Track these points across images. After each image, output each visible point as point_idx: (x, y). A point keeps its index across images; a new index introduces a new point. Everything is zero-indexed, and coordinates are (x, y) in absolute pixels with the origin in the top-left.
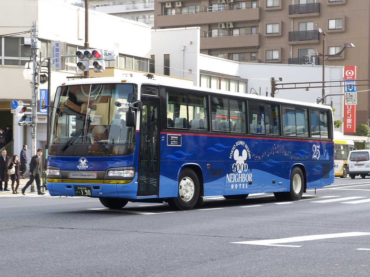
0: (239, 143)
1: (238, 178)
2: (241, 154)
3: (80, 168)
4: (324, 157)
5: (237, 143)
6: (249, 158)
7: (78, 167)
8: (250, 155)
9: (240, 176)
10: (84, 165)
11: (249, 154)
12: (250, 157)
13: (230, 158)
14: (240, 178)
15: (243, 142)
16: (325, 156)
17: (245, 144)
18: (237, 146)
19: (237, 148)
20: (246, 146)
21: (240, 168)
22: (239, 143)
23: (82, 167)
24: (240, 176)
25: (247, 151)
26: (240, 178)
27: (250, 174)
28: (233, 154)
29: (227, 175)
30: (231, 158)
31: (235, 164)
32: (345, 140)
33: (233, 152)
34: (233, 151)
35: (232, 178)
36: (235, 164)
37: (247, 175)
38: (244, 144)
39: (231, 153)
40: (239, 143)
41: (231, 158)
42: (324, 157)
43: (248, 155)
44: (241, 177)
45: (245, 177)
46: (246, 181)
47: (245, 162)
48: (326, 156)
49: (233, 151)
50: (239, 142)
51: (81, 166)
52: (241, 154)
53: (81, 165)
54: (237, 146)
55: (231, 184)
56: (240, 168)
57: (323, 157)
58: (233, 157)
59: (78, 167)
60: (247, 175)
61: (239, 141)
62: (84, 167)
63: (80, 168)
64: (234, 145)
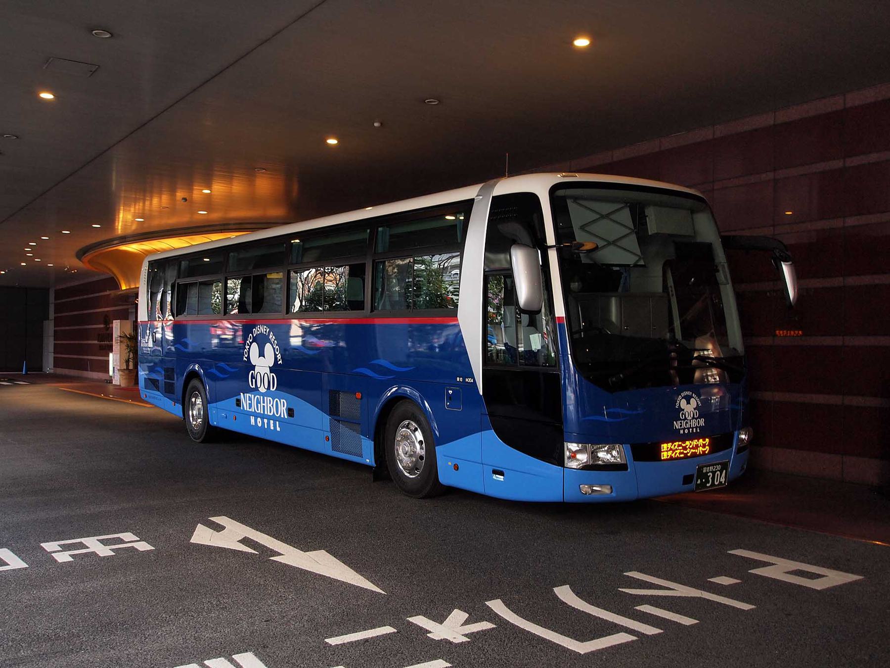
0: (259, 329)
1: (259, 405)
2: (262, 354)
3: (684, 429)
4: (146, 343)
5: (254, 329)
6: (279, 363)
7: (677, 425)
8: (279, 356)
9: (264, 403)
10: (693, 418)
11: (277, 353)
12: (280, 360)
13: (245, 359)
14: (264, 406)
15: (265, 327)
16: (147, 341)
17: (269, 332)
18: (255, 335)
19: (255, 340)
20: (271, 337)
21: (262, 380)
22: (258, 331)
23: (688, 426)
24: (264, 403)
25: (273, 347)
26: (264, 406)
27: (282, 400)
28: (249, 352)
29: (242, 394)
30: (246, 360)
31: (253, 372)
32: (720, 269)
33: (249, 349)
34: (248, 347)
35: (250, 402)
36: (252, 373)
37: (277, 401)
38: (268, 331)
39: (246, 350)
40: (259, 329)
41: (246, 360)
42: (146, 343)
43: (276, 355)
44: (265, 405)
45: (273, 405)
46: (276, 415)
47: (272, 370)
48: (148, 340)
49: (248, 347)
50: (259, 328)
51: (684, 423)
52: (262, 354)
53: (686, 419)
54: (255, 335)
55: (250, 414)
56: (262, 380)
57: (144, 342)
58: (248, 358)
59: (677, 425)
60: (277, 401)
61: (259, 326)
62: (694, 423)
63: (684, 429)
64: (251, 335)
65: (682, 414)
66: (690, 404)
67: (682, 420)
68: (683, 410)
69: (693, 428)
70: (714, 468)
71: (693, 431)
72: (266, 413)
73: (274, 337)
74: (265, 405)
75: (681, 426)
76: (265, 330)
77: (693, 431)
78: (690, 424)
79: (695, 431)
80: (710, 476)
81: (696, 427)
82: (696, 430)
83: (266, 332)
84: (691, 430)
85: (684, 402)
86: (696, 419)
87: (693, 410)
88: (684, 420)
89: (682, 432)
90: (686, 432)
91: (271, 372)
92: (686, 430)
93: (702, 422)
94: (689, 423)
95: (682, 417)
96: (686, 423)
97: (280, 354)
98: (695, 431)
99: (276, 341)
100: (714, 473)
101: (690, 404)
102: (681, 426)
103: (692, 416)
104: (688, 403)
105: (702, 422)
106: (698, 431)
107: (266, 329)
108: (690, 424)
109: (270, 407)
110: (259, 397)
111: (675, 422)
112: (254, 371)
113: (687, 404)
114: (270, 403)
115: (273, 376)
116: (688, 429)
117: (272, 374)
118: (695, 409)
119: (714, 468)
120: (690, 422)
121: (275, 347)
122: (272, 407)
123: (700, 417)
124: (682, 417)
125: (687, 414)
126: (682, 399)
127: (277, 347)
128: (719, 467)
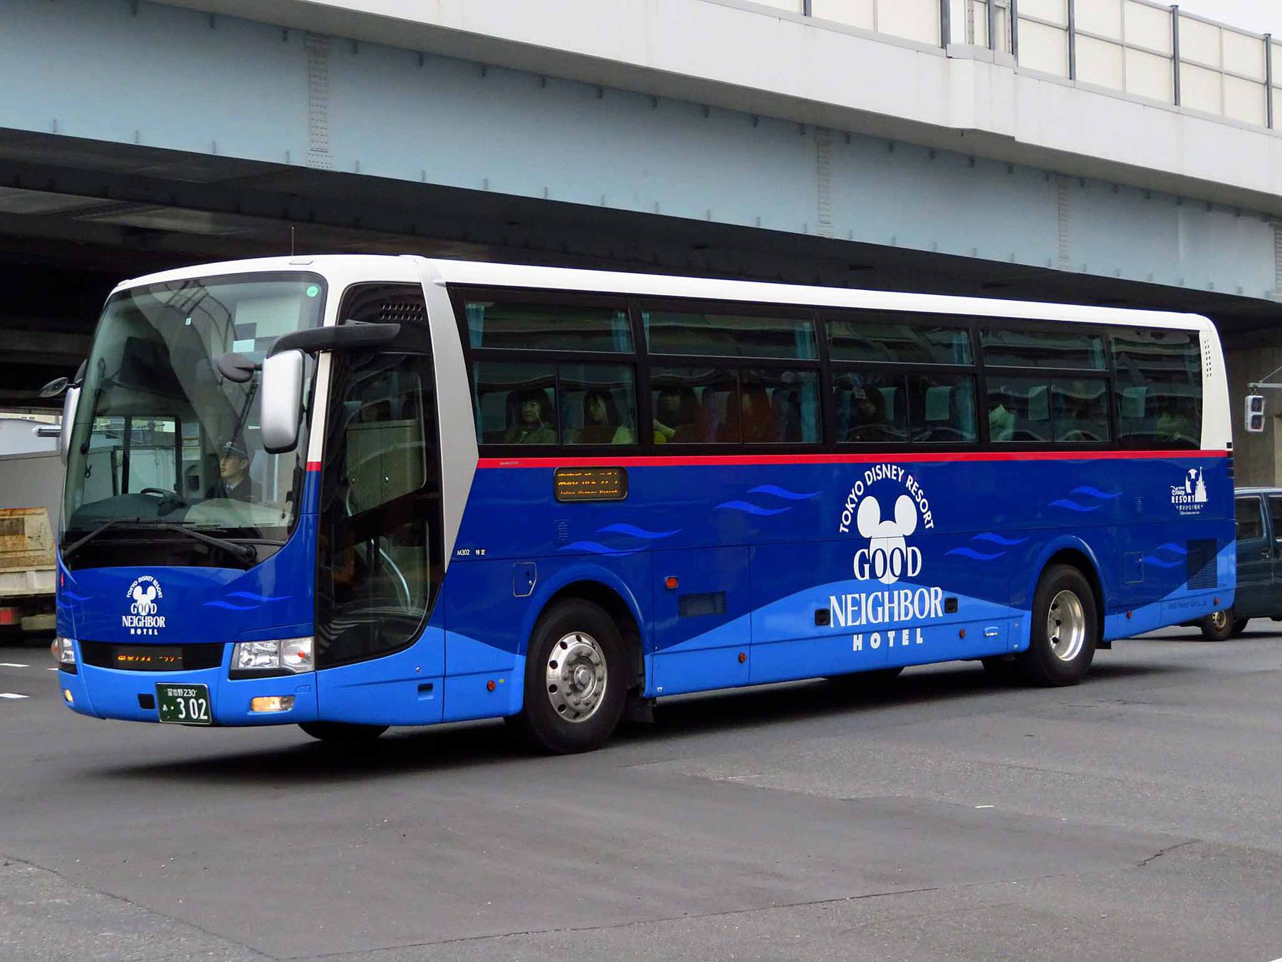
7: (126, 621)
10: (149, 614)
11: (923, 511)
12: (929, 522)
15: (894, 467)
16: (1189, 490)
20: (909, 484)
23: (141, 624)
27: (933, 590)
44: (895, 605)
45: (912, 603)
50: (881, 469)
53: (138, 614)
56: (889, 562)
62: (150, 622)
63: (136, 628)
65: (135, 607)
66: (146, 593)
67: (133, 615)
68: (136, 601)
69: (148, 628)
70: (184, 692)
71: (147, 632)
72: (896, 619)
73: (916, 484)
74: (146, 621)
75: (132, 623)
76: (894, 472)
77: (147, 632)
78: (891, 609)
79: (905, 642)
80: (202, 703)
81: (153, 628)
82: (153, 632)
83: (897, 475)
84: (145, 630)
85: (870, 508)
86: (153, 616)
87: (150, 603)
88: (136, 615)
89: (133, 631)
90: (875, 645)
91: (908, 545)
92: (876, 636)
93: (161, 622)
94: (887, 605)
95: (134, 611)
96: (139, 620)
97: (929, 513)
98: (905, 642)
99: (920, 491)
100: (187, 700)
101: (146, 593)
102: (132, 623)
103: (898, 572)
104: (144, 592)
105: (161, 622)
106: (920, 640)
107: (896, 470)
108: (891, 609)
109: (935, 604)
110: (879, 594)
111: (124, 617)
112: (869, 548)
113: (143, 593)
114: (906, 600)
115: (914, 552)
116: (883, 630)
117: (910, 549)
118: (152, 602)
119: (184, 692)
120: (144, 619)
121: (918, 500)
122: (910, 606)
123: (158, 614)
124: (134, 611)
125: (879, 557)
126: (138, 585)
127: (924, 500)
128: (192, 693)
